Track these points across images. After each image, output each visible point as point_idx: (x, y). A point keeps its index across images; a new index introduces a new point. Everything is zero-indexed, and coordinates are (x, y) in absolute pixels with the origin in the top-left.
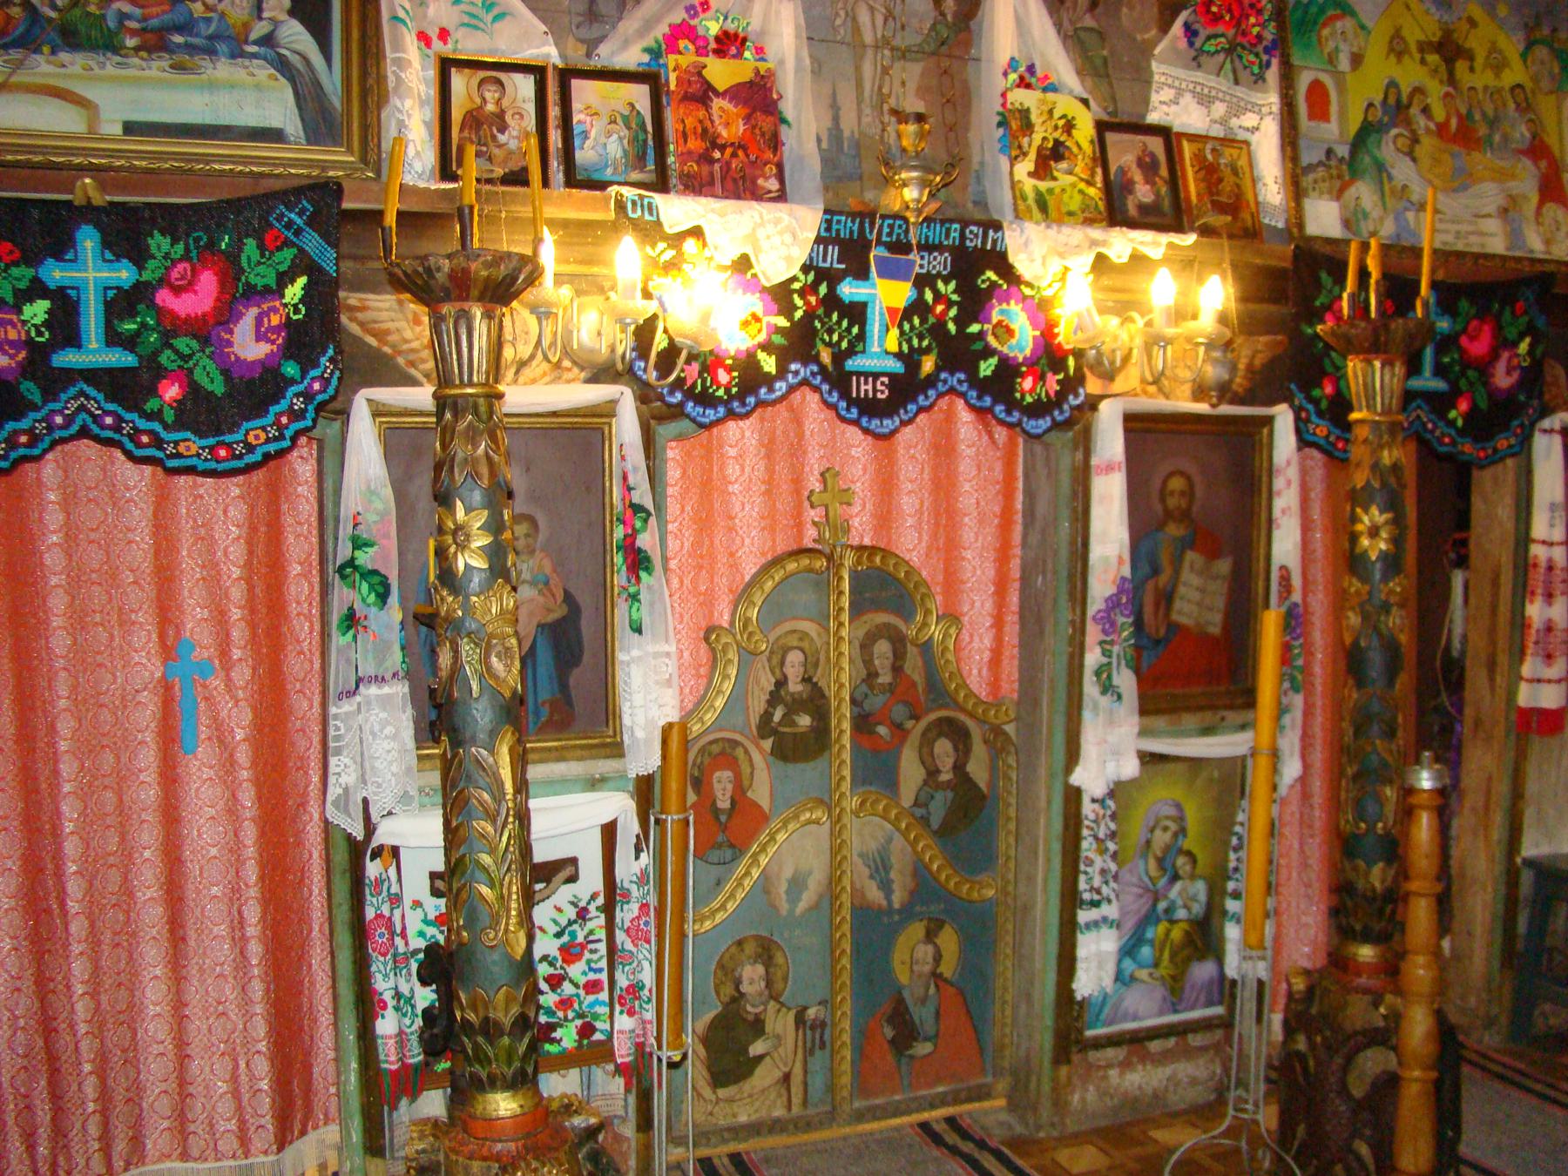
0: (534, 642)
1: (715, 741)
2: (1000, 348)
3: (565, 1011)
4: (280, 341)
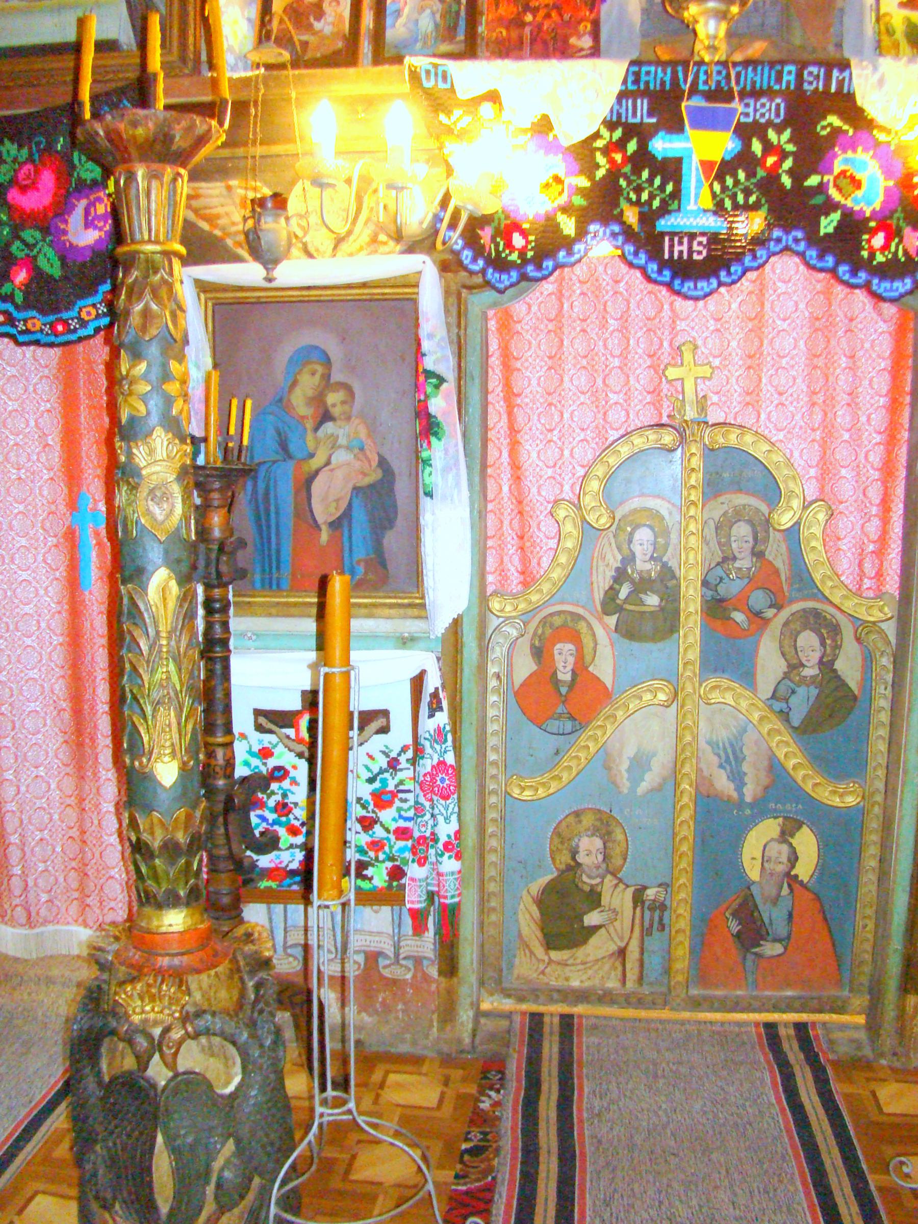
0: (350, 505)
1: (559, 613)
2: (843, 202)
3: (377, 851)
4: (108, 227)
